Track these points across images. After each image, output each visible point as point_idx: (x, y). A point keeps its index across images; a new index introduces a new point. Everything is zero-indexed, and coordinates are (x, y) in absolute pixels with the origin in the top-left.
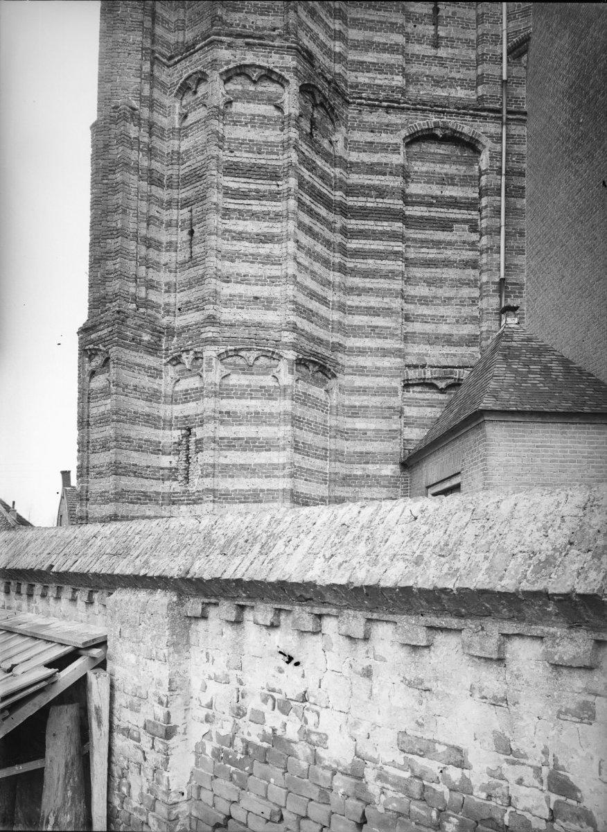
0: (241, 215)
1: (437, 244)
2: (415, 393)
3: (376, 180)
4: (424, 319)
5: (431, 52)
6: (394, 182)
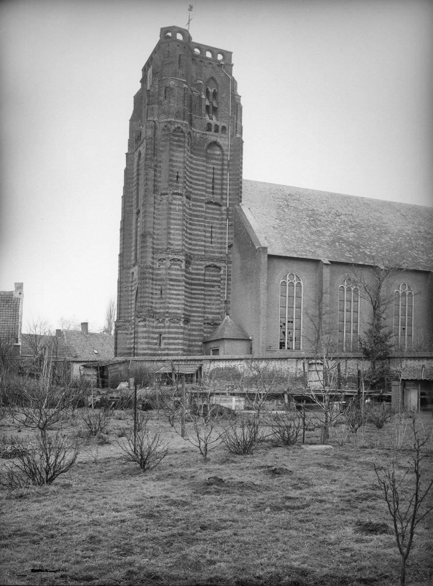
0: (173, 290)
2: (206, 326)
3: (198, 277)
4: (208, 308)
5: (210, 245)
6: (202, 277)
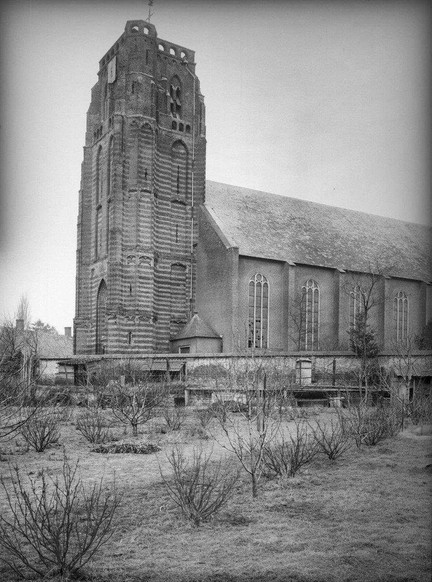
1: (177, 289)
2: (172, 324)
5: (176, 244)
